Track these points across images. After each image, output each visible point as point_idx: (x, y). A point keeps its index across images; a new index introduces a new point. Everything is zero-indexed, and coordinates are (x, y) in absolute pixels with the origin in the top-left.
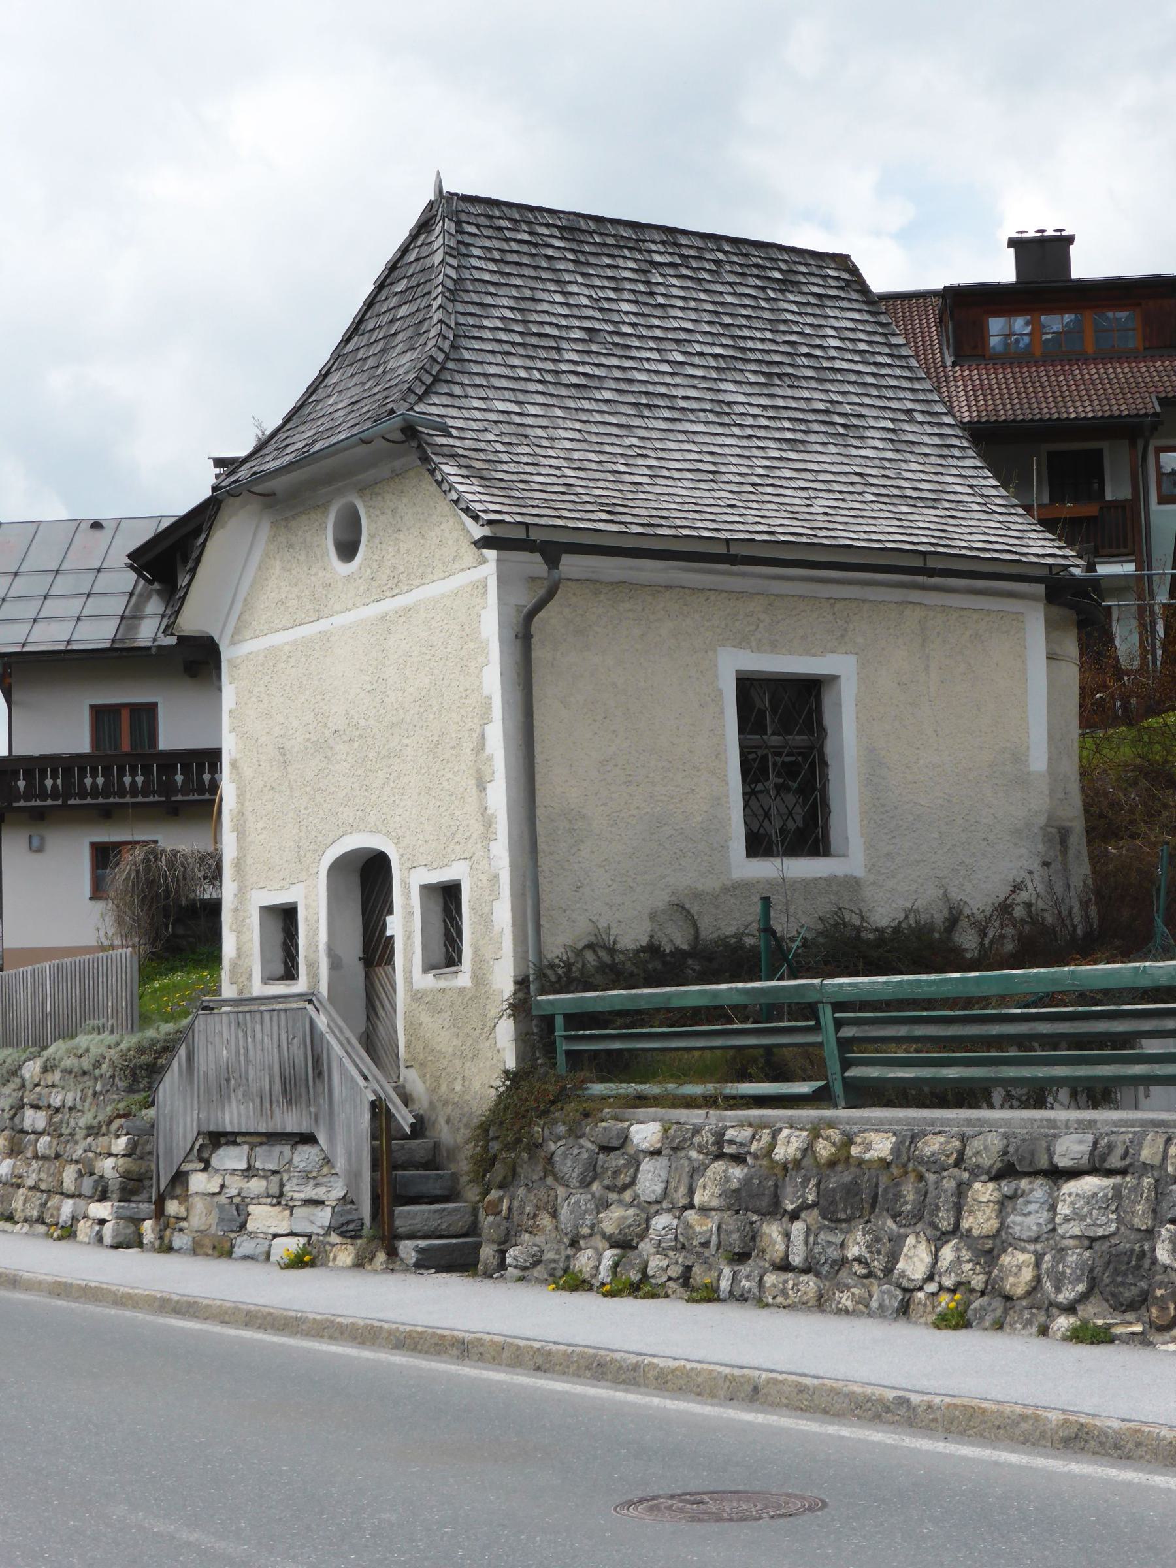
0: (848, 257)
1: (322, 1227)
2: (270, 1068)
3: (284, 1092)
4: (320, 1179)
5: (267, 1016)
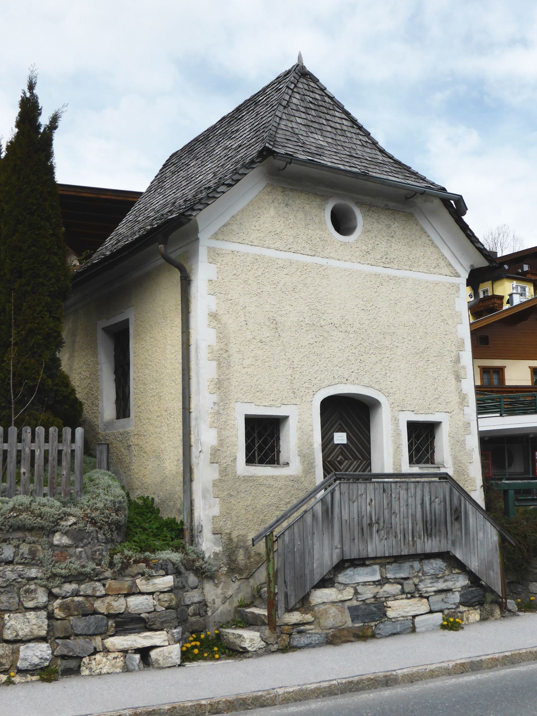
0: (467, 209)
1: (454, 604)
2: (414, 516)
3: (425, 529)
4: (446, 578)
5: (412, 485)
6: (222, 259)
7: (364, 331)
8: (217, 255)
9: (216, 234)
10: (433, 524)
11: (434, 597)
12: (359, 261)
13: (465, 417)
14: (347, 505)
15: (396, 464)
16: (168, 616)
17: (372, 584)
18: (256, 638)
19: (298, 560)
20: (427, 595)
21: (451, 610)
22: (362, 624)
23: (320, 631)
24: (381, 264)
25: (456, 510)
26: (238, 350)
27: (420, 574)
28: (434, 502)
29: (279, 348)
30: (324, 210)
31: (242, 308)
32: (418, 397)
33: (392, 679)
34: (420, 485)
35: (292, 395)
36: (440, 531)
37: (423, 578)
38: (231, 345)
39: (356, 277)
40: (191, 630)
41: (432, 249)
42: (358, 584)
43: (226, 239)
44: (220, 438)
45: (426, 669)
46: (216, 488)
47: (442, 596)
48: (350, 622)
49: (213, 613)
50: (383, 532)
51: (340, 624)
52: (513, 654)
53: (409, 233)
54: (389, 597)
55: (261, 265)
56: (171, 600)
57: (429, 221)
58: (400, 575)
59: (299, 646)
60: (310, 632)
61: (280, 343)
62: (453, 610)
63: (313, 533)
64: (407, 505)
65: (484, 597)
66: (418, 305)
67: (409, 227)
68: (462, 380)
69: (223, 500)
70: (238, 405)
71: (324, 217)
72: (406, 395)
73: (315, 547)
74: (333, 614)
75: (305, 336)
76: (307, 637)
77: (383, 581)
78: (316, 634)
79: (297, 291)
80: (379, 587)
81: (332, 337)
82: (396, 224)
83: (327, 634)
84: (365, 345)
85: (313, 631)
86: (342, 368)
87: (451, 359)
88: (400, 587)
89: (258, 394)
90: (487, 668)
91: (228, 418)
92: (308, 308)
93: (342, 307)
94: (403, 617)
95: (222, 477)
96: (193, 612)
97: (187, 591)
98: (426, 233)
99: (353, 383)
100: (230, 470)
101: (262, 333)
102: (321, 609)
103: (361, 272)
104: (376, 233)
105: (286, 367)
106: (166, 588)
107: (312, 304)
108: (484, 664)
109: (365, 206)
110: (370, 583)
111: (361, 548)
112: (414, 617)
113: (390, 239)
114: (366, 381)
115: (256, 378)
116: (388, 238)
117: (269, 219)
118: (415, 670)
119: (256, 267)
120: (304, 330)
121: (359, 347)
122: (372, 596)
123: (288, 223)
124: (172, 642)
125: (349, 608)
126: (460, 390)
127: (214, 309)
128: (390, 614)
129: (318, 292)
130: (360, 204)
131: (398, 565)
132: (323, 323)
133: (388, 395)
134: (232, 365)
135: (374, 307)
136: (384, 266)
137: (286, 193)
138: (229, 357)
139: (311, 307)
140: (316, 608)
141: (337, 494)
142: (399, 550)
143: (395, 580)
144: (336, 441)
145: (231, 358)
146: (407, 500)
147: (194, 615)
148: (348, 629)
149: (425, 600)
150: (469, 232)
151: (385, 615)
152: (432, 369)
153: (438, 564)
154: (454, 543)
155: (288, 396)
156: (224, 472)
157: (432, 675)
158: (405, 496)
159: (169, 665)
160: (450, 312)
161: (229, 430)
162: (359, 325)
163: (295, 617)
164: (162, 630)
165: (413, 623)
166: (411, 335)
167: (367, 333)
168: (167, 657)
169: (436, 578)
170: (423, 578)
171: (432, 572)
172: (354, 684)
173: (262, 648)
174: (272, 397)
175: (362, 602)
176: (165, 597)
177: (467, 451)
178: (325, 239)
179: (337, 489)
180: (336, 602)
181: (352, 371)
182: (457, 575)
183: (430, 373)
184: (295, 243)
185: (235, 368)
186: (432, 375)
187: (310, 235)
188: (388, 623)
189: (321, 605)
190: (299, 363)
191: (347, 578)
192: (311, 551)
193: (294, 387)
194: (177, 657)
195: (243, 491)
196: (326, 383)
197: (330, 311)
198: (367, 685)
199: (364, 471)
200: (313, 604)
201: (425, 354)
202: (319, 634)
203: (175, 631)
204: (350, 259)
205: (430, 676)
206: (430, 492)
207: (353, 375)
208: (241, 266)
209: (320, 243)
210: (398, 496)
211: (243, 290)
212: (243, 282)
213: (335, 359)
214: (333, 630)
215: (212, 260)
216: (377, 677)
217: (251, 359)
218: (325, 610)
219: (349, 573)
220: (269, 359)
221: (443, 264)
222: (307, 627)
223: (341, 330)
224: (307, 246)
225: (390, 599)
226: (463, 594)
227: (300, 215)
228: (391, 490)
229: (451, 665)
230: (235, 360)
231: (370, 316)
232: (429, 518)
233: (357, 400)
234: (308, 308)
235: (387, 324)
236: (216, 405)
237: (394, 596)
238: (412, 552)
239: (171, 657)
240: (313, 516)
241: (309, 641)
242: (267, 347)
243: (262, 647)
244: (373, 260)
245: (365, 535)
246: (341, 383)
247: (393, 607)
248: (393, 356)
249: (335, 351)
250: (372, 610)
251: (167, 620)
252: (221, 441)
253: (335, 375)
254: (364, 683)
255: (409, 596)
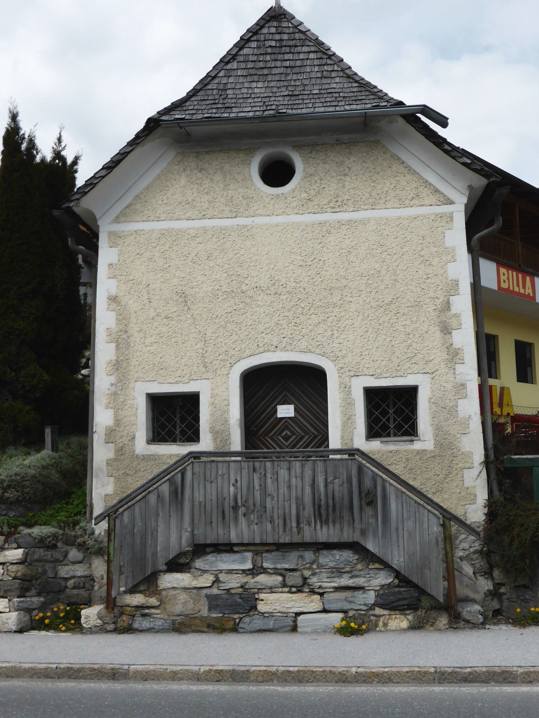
0: (447, 119)
1: (365, 605)
6: (124, 241)
7: (301, 289)
8: (118, 238)
9: (117, 217)
10: (331, 509)
11: (332, 594)
12: (296, 212)
13: (457, 377)
14: (202, 486)
15: (345, 438)
16: (12, 585)
17: (240, 572)
18: (92, 616)
19: (138, 541)
20: (321, 591)
21: (360, 612)
22: (221, 615)
23: (166, 617)
24: (329, 210)
25: (368, 493)
26: (140, 329)
27: (314, 566)
28: (332, 482)
29: (189, 322)
30: (250, 164)
31: (145, 287)
32: (381, 358)
33: (121, 673)
34: (263, 463)
35: (204, 369)
36: (341, 517)
37: (317, 571)
38: (132, 325)
39: (291, 230)
40: (67, 602)
41: (409, 177)
42: (221, 571)
43: (128, 220)
44: (116, 418)
45: (167, 669)
46: (110, 468)
47: (348, 594)
48: (206, 612)
49: (100, 588)
50: (252, 516)
51: (191, 612)
52: (301, 671)
53: (371, 166)
54: (264, 589)
55: (169, 239)
56: (17, 572)
57: (398, 142)
58: (283, 565)
59: (140, 629)
60: (156, 616)
61: (189, 316)
62: (363, 612)
63: (158, 515)
64: (289, 487)
65: (420, 600)
66: (384, 248)
67: (372, 158)
68: (453, 331)
69: (117, 479)
70: (138, 384)
71: (249, 172)
72: (362, 357)
73: (159, 529)
74: (183, 601)
75: (221, 305)
76: (150, 621)
77: (254, 572)
78: (161, 619)
79: (212, 259)
80: (251, 576)
81: (255, 303)
82: (352, 159)
83: (174, 621)
84: (303, 305)
85: (159, 616)
86: (270, 335)
87: (434, 307)
88: (280, 578)
89: (161, 372)
90: (257, 682)
91: (127, 398)
92: (226, 275)
93: (272, 267)
94: (282, 613)
95: (117, 456)
96: (73, 585)
97: (66, 565)
98: (399, 159)
99: (284, 349)
100: (128, 449)
101: (168, 308)
102: (169, 594)
103: (299, 224)
104: (322, 175)
105: (197, 340)
106: (14, 560)
107: (230, 269)
108: (251, 675)
109: (306, 148)
110: (237, 572)
111: (221, 532)
112: (298, 614)
113: (343, 178)
114: (303, 344)
115: (160, 355)
116: (340, 177)
117: (180, 189)
118: (152, 667)
119: (163, 242)
120: (220, 300)
121: (294, 308)
122: (239, 585)
123: (202, 189)
124: (12, 610)
125: (207, 596)
126: (448, 344)
127: (114, 292)
128: (261, 607)
129: (239, 255)
130: (298, 147)
131: (281, 553)
132: (244, 288)
133: (335, 359)
134: (132, 345)
135: (317, 260)
136: (333, 210)
137: (201, 157)
138: (129, 337)
139: (230, 273)
140: (164, 593)
141: (189, 475)
142: (276, 537)
143: (276, 571)
144: (279, 415)
145: (131, 338)
146: (290, 480)
147: (74, 588)
148: (202, 618)
149: (317, 597)
150: (447, 147)
151: (255, 608)
152: (403, 323)
153: (347, 555)
154: (363, 532)
155: (198, 371)
156: (120, 451)
157: (174, 676)
158: (287, 477)
159: (6, 630)
160: (435, 249)
161: (127, 410)
162: (294, 284)
163: (137, 599)
164: (6, 598)
165: (295, 621)
166: (372, 286)
167: (305, 292)
168: (4, 622)
169: (338, 572)
170: (317, 571)
171: (332, 564)
172: (74, 671)
173: (98, 626)
174: (179, 373)
175: (226, 592)
176: (14, 568)
177: (459, 419)
178: (250, 196)
179: (189, 468)
180: (189, 589)
181: (283, 336)
182: (376, 571)
183: (401, 328)
184: (211, 209)
185: (135, 348)
186: (403, 330)
187: (230, 196)
188: (258, 617)
189: (171, 590)
190: (213, 335)
191: (206, 564)
192: (155, 533)
193: (206, 360)
194: (13, 624)
195: (143, 469)
196: (248, 352)
197: (255, 274)
198: (89, 675)
199: (319, 447)
200: (161, 588)
201: (393, 306)
202: (164, 620)
203: (15, 600)
204: (284, 212)
205: (170, 677)
206: (326, 472)
207: (284, 342)
208: (145, 245)
209: (244, 201)
210: (275, 476)
211: (147, 267)
212: (147, 260)
213: (260, 325)
214: (182, 617)
215: (112, 244)
216: (102, 668)
217: (154, 337)
218: (174, 595)
219: (211, 558)
220: (176, 335)
221: (425, 192)
222: (153, 611)
223: (269, 292)
224: (227, 209)
225: (264, 591)
226: (382, 594)
227: (218, 177)
228: (265, 470)
229: (202, 670)
230: (135, 339)
231: (310, 271)
232: (323, 502)
233: (260, 369)
234: (226, 275)
235: (336, 278)
236: (114, 386)
237: (271, 588)
238: (296, 539)
239: (8, 623)
240: (159, 496)
241: (152, 626)
242: (173, 323)
243: (99, 625)
244: (316, 207)
245: (227, 519)
246: (268, 351)
247: (268, 600)
248: (343, 314)
249: (261, 317)
250: (236, 601)
251: (10, 589)
252: (118, 422)
253: (260, 344)
254: (85, 672)
255: (294, 590)
